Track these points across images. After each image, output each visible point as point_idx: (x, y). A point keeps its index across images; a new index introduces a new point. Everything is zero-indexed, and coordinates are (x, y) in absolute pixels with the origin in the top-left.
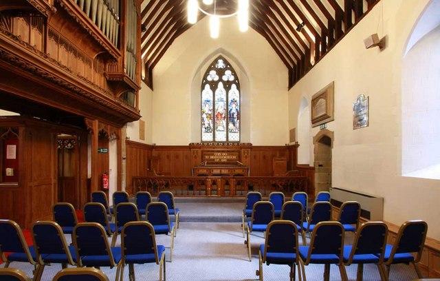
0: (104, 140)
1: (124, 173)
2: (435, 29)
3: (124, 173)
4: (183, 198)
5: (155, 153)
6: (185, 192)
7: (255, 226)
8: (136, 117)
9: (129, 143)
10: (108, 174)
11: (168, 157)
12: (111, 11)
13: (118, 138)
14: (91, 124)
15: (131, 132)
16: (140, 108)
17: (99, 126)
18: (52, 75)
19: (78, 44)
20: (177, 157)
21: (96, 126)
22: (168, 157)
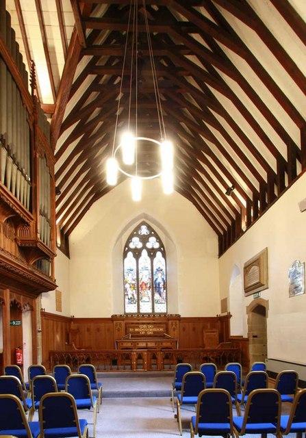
0: (16, 311)
1: (40, 347)
3: (40, 347)
6: (108, 367)
9: (44, 314)
10: (21, 348)
11: (88, 330)
13: (32, 310)
15: (47, 303)
20: (98, 330)
22: (88, 330)
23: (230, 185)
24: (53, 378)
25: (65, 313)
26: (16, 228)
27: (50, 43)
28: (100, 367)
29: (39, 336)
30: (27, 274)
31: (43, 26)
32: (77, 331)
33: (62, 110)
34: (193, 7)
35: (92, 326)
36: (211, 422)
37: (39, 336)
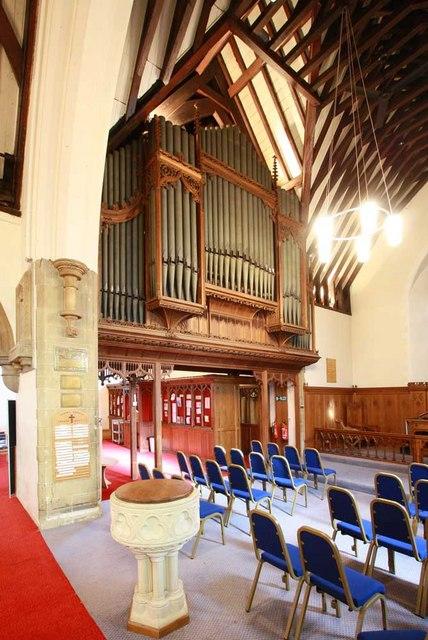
0: (281, 390)
1: (303, 424)
2: (379, 221)
3: (303, 424)
4: (370, 461)
5: (356, 397)
6: (399, 456)
7: (75, 447)
8: (315, 360)
9: (307, 389)
10: (287, 424)
11: (375, 403)
12: (264, 269)
13: (295, 385)
14: (260, 376)
15: (313, 377)
16: (317, 348)
17: (269, 376)
18: (214, 348)
19: (235, 314)
20: (389, 403)
21: (265, 377)
22: (375, 403)
23: (106, 294)
24: (239, 451)
25: (341, 383)
26: (265, 317)
27: (290, 123)
28: (388, 454)
29: (302, 412)
30: (277, 356)
31: (267, 126)
32: (362, 405)
33: (308, 176)
34: (310, 21)
35: (381, 398)
36: (399, 540)
37: (302, 412)
